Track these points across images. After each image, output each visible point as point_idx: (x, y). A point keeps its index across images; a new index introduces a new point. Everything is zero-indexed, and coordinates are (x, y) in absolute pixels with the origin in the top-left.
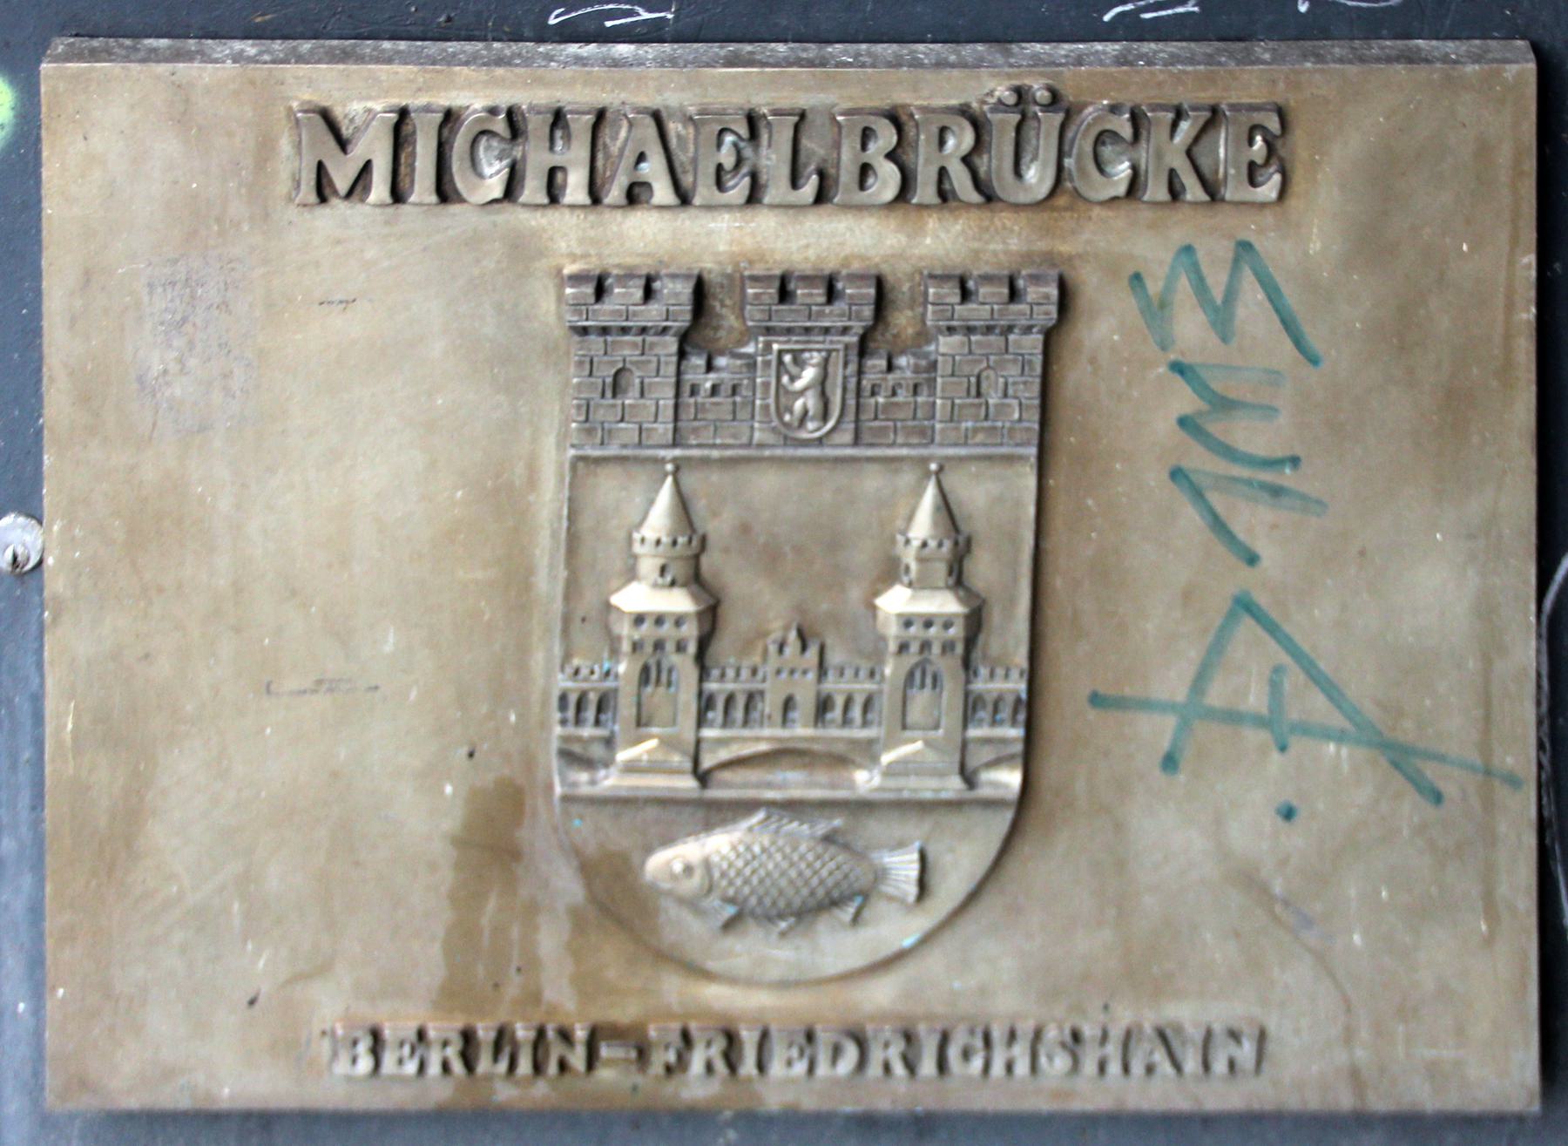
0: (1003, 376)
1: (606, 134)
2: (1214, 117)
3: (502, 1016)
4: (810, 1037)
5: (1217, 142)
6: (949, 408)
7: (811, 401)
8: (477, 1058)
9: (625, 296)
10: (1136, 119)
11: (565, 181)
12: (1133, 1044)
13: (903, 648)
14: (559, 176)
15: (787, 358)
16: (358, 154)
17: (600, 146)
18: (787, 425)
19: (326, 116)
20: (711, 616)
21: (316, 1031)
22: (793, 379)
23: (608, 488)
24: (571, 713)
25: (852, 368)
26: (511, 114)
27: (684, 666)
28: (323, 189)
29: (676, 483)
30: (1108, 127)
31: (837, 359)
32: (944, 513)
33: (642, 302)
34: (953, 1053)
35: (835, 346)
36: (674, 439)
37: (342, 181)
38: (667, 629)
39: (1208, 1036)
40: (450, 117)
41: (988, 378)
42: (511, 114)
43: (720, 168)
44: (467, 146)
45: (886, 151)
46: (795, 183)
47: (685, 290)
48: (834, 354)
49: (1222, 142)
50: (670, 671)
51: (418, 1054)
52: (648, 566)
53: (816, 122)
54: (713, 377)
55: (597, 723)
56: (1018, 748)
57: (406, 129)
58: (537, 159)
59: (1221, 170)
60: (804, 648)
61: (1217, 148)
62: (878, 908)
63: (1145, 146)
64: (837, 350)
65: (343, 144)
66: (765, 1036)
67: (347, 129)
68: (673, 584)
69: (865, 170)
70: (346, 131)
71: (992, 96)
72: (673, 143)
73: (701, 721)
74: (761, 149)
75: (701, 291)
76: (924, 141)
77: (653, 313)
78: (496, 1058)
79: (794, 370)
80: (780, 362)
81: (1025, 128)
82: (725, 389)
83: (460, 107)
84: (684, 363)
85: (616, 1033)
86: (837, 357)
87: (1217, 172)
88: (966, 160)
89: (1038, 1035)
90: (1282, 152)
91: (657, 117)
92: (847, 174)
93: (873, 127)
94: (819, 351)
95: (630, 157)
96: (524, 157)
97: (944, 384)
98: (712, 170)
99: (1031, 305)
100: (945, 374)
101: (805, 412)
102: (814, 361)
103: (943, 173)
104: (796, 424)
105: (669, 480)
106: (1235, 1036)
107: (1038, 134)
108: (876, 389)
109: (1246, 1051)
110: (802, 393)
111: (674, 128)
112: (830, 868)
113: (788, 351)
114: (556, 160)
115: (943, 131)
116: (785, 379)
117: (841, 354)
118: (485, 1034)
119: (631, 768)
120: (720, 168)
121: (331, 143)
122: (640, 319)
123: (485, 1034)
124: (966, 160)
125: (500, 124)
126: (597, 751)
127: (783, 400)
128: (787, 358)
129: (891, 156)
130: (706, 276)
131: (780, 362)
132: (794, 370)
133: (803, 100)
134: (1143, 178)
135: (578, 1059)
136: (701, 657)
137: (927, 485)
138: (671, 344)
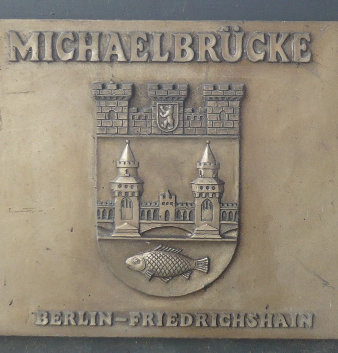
0: (227, 114)
1: (103, 40)
2: (289, 37)
3: (86, 309)
4: (178, 316)
5: (291, 44)
6: (211, 123)
7: (169, 120)
8: (78, 320)
9: (111, 87)
10: (266, 37)
11: (91, 55)
12: (275, 318)
13: (200, 195)
14: (89, 53)
15: (161, 107)
16: (27, 45)
17: (101, 43)
18: (162, 128)
19: (18, 34)
20: (141, 183)
21: (30, 312)
22: (163, 113)
23: (108, 147)
24: (101, 216)
25: (182, 110)
26: (74, 34)
27: (135, 201)
28: (18, 58)
29: (129, 147)
30: (257, 38)
31: (177, 108)
32: (211, 155)
33: (116, 89)
34: (221, 320)
35: (176, 103)
36: (128, 132)
37: (23, 54)
38: (129, 189)
39: (297, 316)
40: (54, 36)
41: (223, 115)
42: (74, 34)
43: (138, 49)
44: (61, 43)
45: (189, 45)
46: (162, 54)
47: (129, 87)
48: (176, 106)
49: (292, 45)
50: (130, 202)
51: (61, 319)
52: (122, 171)
53: (168, 37)
54: (139, 114)
55: (109, 219)
56: (237, 227)
57: (42, 39)
58: (82, 47)
59: (292, 54)
60: (171, 198)
61: (291, 46)
62: (195, 274)
63: (268, 45)
64: (176, 105)
65: (23, 43)
66: (164, 315)
67: (24, 38)
68: (130, 176)
69: (183, 51)
70: (24, 40)
71: (221, 29)
72: (124, 43)
73: (140, 219)
74: (151, 45)
75: (134, 88)
76: (201, 42)
77: (119, 92)
78: (84, 320)
79: (163, 111)
80: (159, 108)
81: (232, 39)
82: (143, 118)
83: (58, 32)
84: (130, 109)
85: (121, 314)
86: (177, 107)
87: (291, 54)
88: (214, 48)
89: (246, 316)
90: (313, 49)
91: (118, 34)
92: (177, 53)
93: (185, 37)
94: (171, 105)
95: (110, 48)
96: (78, 47)
97: (209, 116)
98: (136, 52)
99: (235, 91)
100: (210, 113)
101: (168, 124)
102: (169, 108)
103: (207, 52)
104: (165, 127)
105: (127, 145)
106: (306, 317)
107: (236, 41)
108: (189, 118)
109: (309, 322)
110: (166, 118)
111: (124, 39)
112: (181, 264)
113: (161, 105)
114: (88, 47)
115: (207, 39)
116: (161, 114)
117: (178, 106)
118: (81, 314)
119: (119, 231)
120: (138, 49)
121: (19, 42)
122: (116, 94)
123: (81, 314)
124: (214, 48)
125: (71, 37)
126: (109, 227)
127: (161, 120)
128: (161, 107)
129: (190, 46)
130: (135, 84)
131: (159, 108)
132: (163, 111)
133: (163, 30)
134: (268, 55)
135: (109, 321)
136: (139, 197)
137: (206, 147)
138: (126, 103)
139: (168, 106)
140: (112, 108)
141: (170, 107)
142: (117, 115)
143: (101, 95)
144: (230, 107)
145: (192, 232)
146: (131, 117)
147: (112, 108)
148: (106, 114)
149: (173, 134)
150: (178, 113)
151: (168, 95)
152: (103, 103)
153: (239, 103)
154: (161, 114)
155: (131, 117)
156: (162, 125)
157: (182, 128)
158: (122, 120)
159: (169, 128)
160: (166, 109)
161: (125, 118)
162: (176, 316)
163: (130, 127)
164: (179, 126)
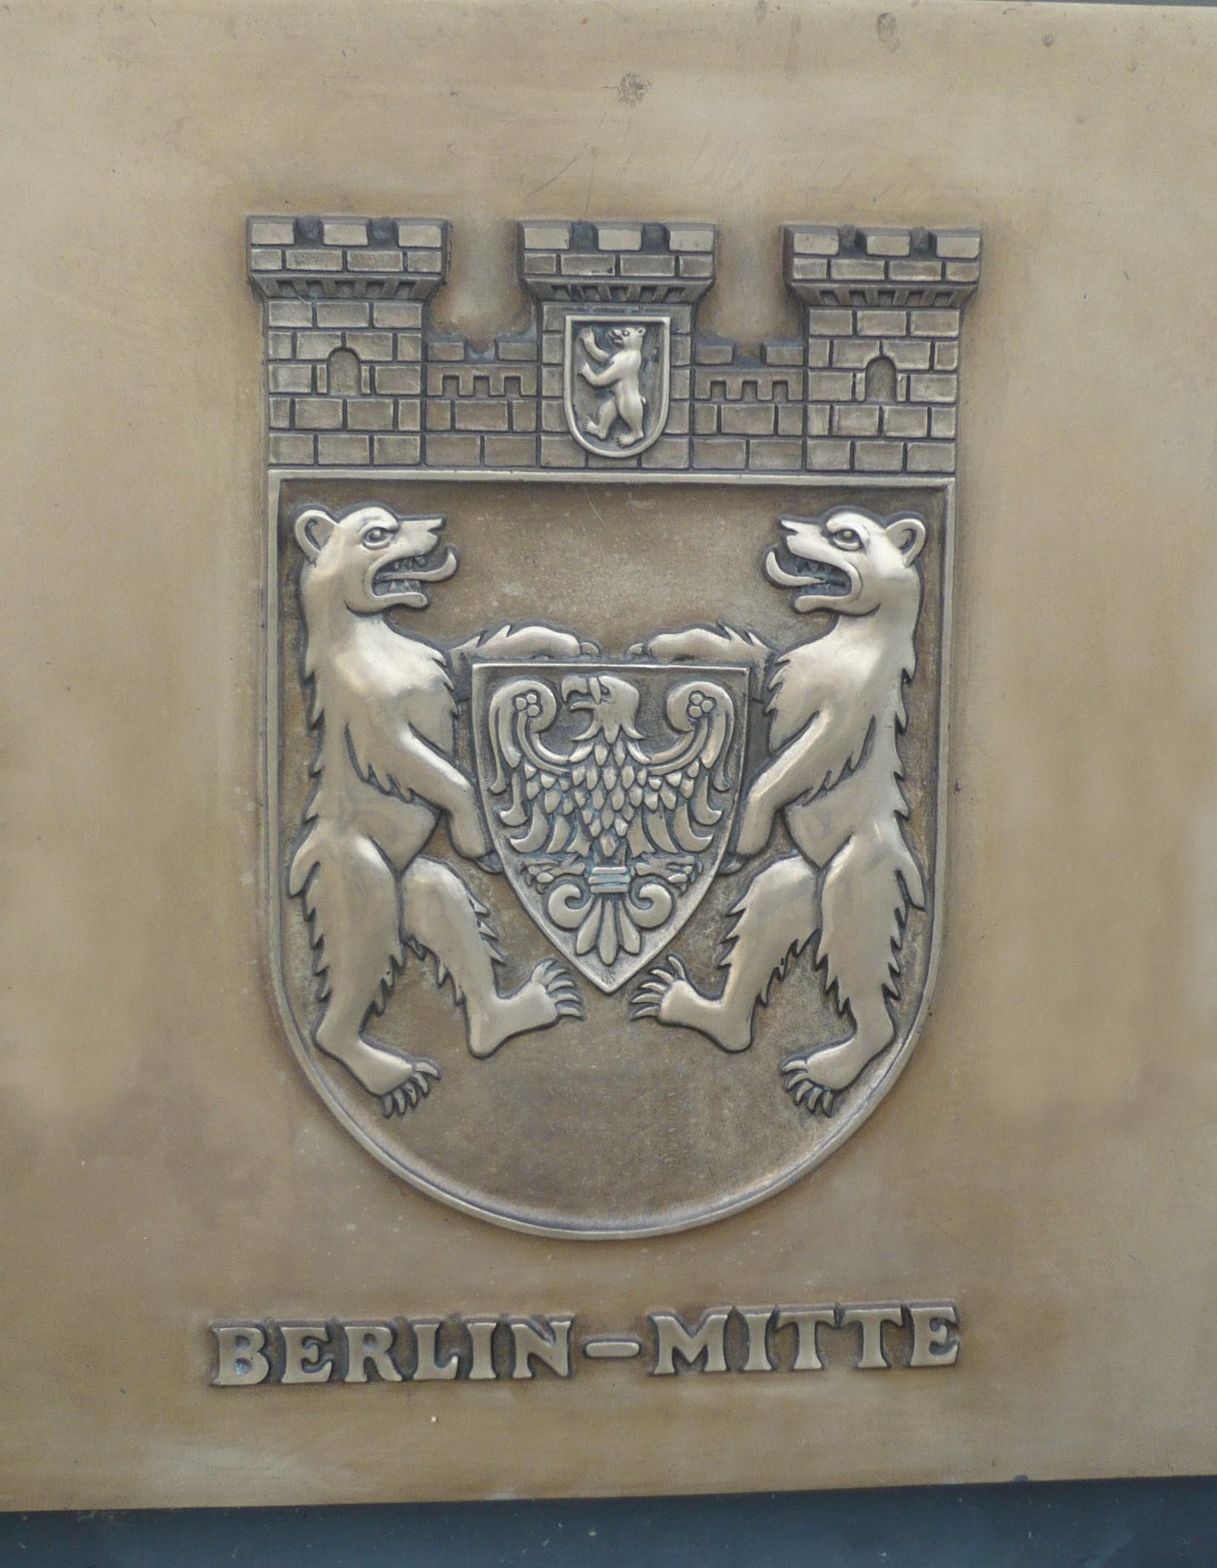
15: (589, 338)
116: (586, 369)
128: (589, 338)
139: (618, 332)
140: (343, 338)
141: (634, 334)
142: (372, 371)
143: (294, 271)
144: (792, 401)
145: (758, 666)
146: (436, 382)
147: (343, 338)
148: (314, 370)
149: (639, 468)
150: (932, 334)
151: (677, 276)
152: (291, 315)
153: (689, 312)
154: (586, 369)
155: (436, 382)
156: (591, 426)
157: (685, 441)
158: (396, 397)
159: (627, 439)
160: (616, 346)
161: (411, 388)
162: (324, 1338)
163: (432, 431)
164: (590, 456)
